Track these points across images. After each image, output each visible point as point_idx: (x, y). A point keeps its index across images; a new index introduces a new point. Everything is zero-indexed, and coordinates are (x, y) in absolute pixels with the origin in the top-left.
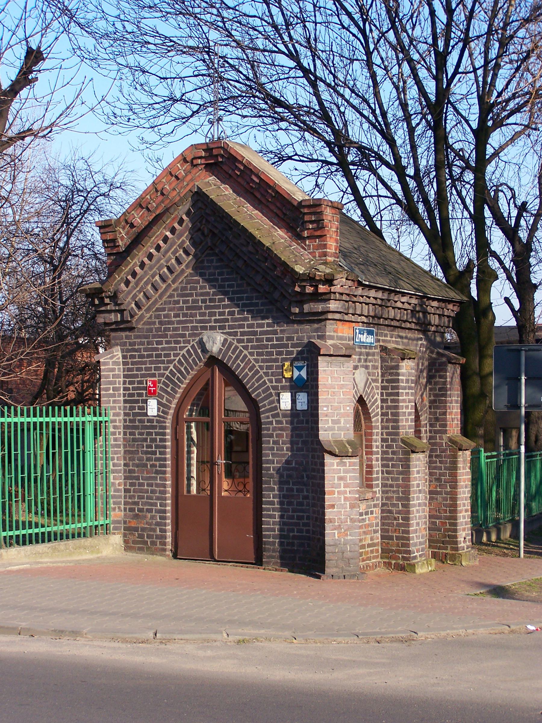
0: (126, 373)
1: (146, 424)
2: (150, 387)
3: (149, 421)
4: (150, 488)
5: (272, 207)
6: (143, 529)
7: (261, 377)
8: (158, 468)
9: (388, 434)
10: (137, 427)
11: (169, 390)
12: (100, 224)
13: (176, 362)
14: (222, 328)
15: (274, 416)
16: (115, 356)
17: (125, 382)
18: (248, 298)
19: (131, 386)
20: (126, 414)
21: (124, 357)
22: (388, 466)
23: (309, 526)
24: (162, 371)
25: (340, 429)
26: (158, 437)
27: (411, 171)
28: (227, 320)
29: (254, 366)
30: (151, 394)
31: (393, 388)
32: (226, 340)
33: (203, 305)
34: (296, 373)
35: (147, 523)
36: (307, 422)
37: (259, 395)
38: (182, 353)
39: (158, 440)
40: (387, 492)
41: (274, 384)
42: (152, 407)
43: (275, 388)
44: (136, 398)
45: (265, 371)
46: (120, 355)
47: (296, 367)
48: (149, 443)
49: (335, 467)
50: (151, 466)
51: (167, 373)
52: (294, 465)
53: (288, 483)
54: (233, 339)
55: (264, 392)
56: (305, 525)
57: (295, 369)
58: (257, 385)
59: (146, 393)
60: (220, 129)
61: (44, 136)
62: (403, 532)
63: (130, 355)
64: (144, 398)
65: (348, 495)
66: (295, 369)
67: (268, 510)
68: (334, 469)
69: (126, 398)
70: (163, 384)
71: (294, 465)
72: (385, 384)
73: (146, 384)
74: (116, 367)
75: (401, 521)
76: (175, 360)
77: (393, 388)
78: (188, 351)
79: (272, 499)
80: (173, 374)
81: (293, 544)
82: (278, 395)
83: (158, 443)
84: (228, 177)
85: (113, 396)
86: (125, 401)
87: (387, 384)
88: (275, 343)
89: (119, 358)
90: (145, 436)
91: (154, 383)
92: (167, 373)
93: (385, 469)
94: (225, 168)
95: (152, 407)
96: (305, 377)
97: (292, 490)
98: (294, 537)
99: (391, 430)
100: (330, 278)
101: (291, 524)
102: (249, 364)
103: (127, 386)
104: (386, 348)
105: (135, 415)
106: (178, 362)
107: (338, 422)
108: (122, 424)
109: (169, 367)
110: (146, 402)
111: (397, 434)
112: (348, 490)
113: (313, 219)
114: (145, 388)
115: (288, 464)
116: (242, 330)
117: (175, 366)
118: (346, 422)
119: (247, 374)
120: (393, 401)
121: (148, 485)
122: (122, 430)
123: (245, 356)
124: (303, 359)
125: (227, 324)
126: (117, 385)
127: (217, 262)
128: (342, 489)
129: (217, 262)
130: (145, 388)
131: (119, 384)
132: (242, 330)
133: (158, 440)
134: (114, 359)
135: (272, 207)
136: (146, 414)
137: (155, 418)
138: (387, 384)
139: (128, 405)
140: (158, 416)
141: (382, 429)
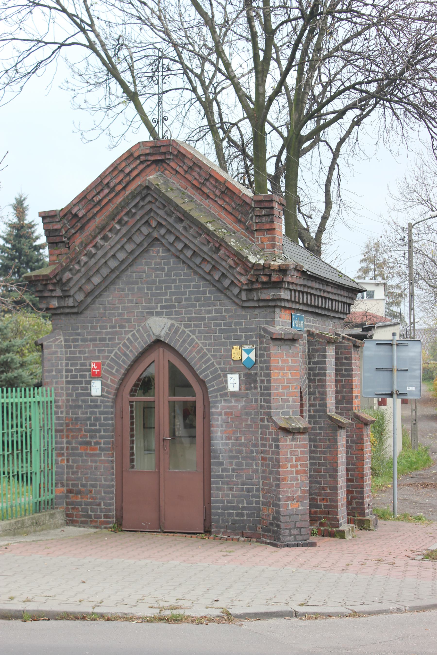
0: (68, 355)
1: (90, 403)
2: (94, 368)
3: (92, 401)
4: (94, 464)
5: (220, 202)
6: (87, 504)
7: (209, 360)
8: (102, 445)
9: (316, 411)
10: (80, 407)
11: (114, 371)
12: (43, 215)
13: (121, 345)
14: (169, 314)
15: (221, 396)
16: (57, 339)
17: (67, 365)
18: (195, 286)
19: (73, 368)
20: (68, 395)
21: (66, 341)
22: (315, 440)
23: (259, 498)
24: (106, 354)
25: (289, 407)
26: (102, 416)
27: (128, 178)
28: (174, 307)
29: (202, 349)
30: (96, 376)
31: (320, 369)
32: (172, 325)
33: (149, 292)
34: (245, 356)
35: (92, 498)
36: (256, 401)
37: (207, 376)
38: (127, 337)
39: (102, 419)
40: (314, 464)
41: (222, 366)
42: (96, 388)
43: (222, 370)
44: (79, 379)
45: (213, 353)
46: (62, 339)
47: (244, 350)
48: (93, 422)
49: (288, 443)
50: (95, 443)
51: (112, 355)
52: (243, 441)
53: (237, 457)
54: (181, 324)
55: (212, 373)
56: (254, 496)
57: (243, 351)
58: (204, 366)
59: (89, 375)
60: (165, 129)
61: (407, 110)
62: (331, 501)
63: (72, 339)
64: (88, 379)
65: (299, 468)
66: (243, 352)
67: (217, 483)
68: (287, 445)
69: (69, 379)
70: (107, 366)
71: (243, 441)
72: (312, 365)
73: (90, 365)
74: (59, 350)
75: (328, 491)
76: (120, 343)
77: (320, 369)
78: (134, 335)
79: (220, 473)
80: (119, 357)
81: (242, 515)
82: (226, 376)
83: (102, 421)
84: (174, 172)
85: (55, 377)
86: (68, 382)
87: (314, 366)
88: (223, 327)
89: (61, 341)
90: (88, 415)
91: (98, 365)
92: (112, 355)
93: (312, 444)
94: (172, 164)
95: (96, 388)
96: (253, 359)
97: (241, 464)
98: (244, 508)
99: (318, 408)
100: (284, 268)
101: (241, 496)
102: (197, 348)
103: (70, 367)
104: (313, 333)
105: (78, 395)
106: (123, 345)
107: (288, 401)
108: (64, 404)
109: (114, 350)
110: (89, 383)
111: (325, 411)
112: (299, 463)
113: (263, 213)
114: (89, 370)
115: (237, 440)
116: (189, 316)
117: (119, 349)
118: (294, 401)
119: (195, 357)
120: (319, 381)
121: (92, 461)
122: (64, 410)
123: (193, 340)
124: (252, 343)
125: (174, 310)
126: (60, 367)
127: (162, 253)
128: (294, 463)
129: (162, 253)
130: (89, 370)
131: (62, 366)
132: (189, 316)
133: (102, 419)
134: (56, 343)
135: (220, 202)
136: (90, 395)
137: (99, 398)
138: (314, 366)
139: (71, 386)
140: (102, 396)
141: (309, 407)
